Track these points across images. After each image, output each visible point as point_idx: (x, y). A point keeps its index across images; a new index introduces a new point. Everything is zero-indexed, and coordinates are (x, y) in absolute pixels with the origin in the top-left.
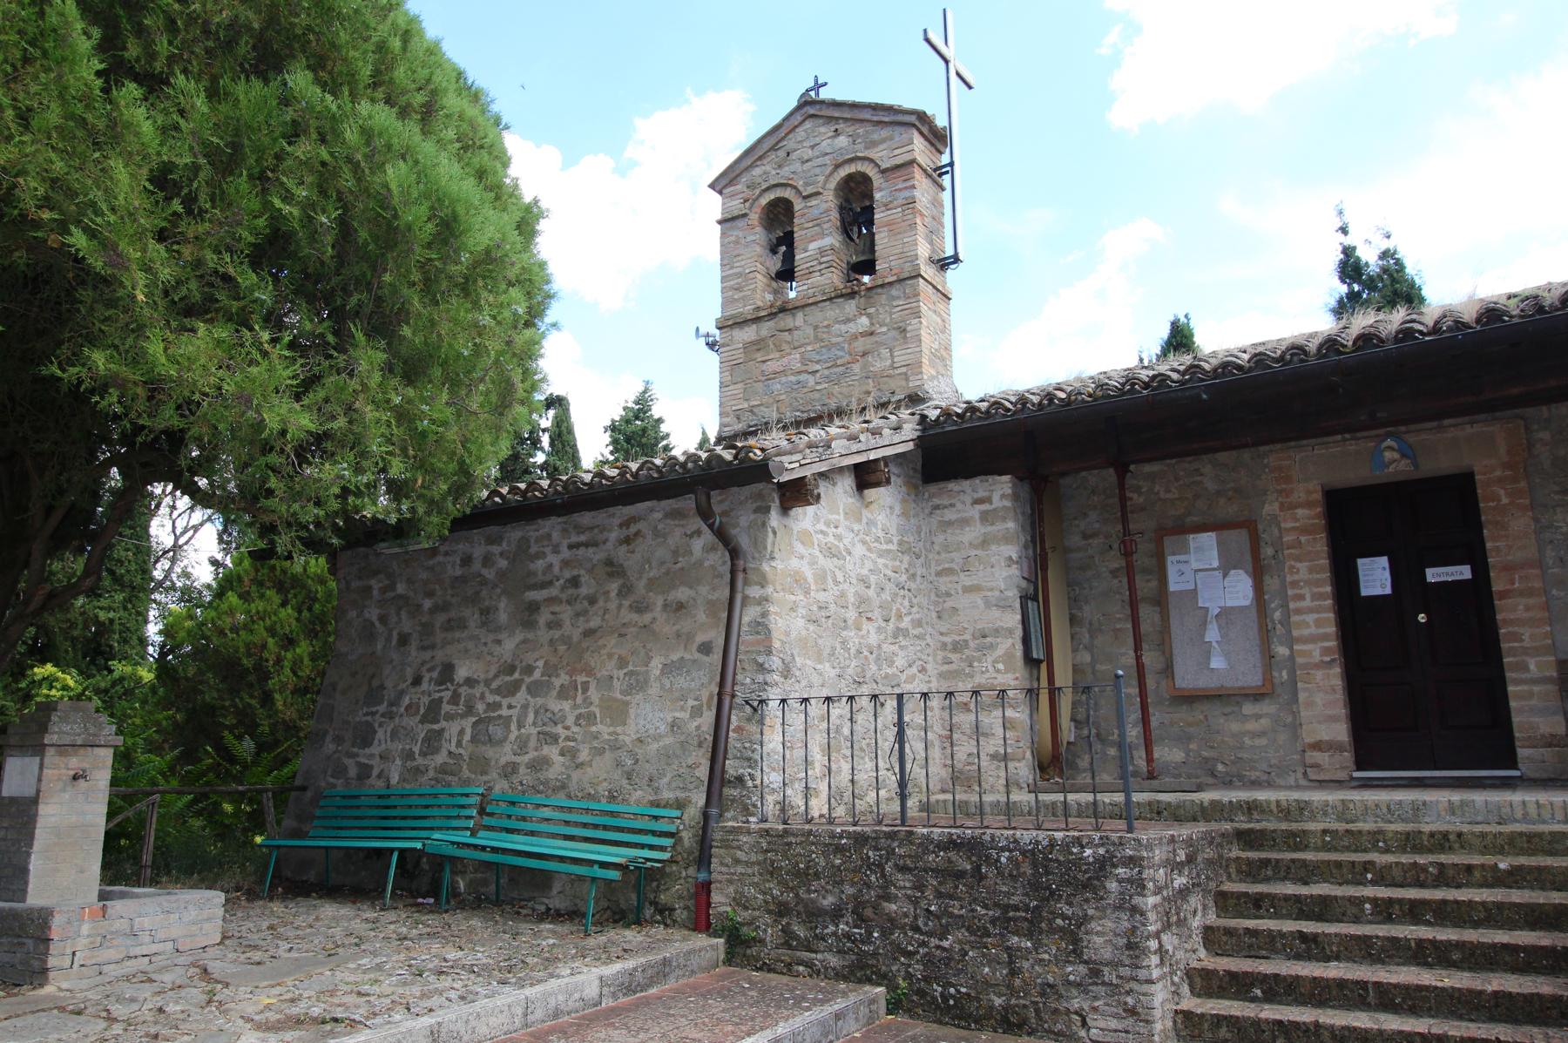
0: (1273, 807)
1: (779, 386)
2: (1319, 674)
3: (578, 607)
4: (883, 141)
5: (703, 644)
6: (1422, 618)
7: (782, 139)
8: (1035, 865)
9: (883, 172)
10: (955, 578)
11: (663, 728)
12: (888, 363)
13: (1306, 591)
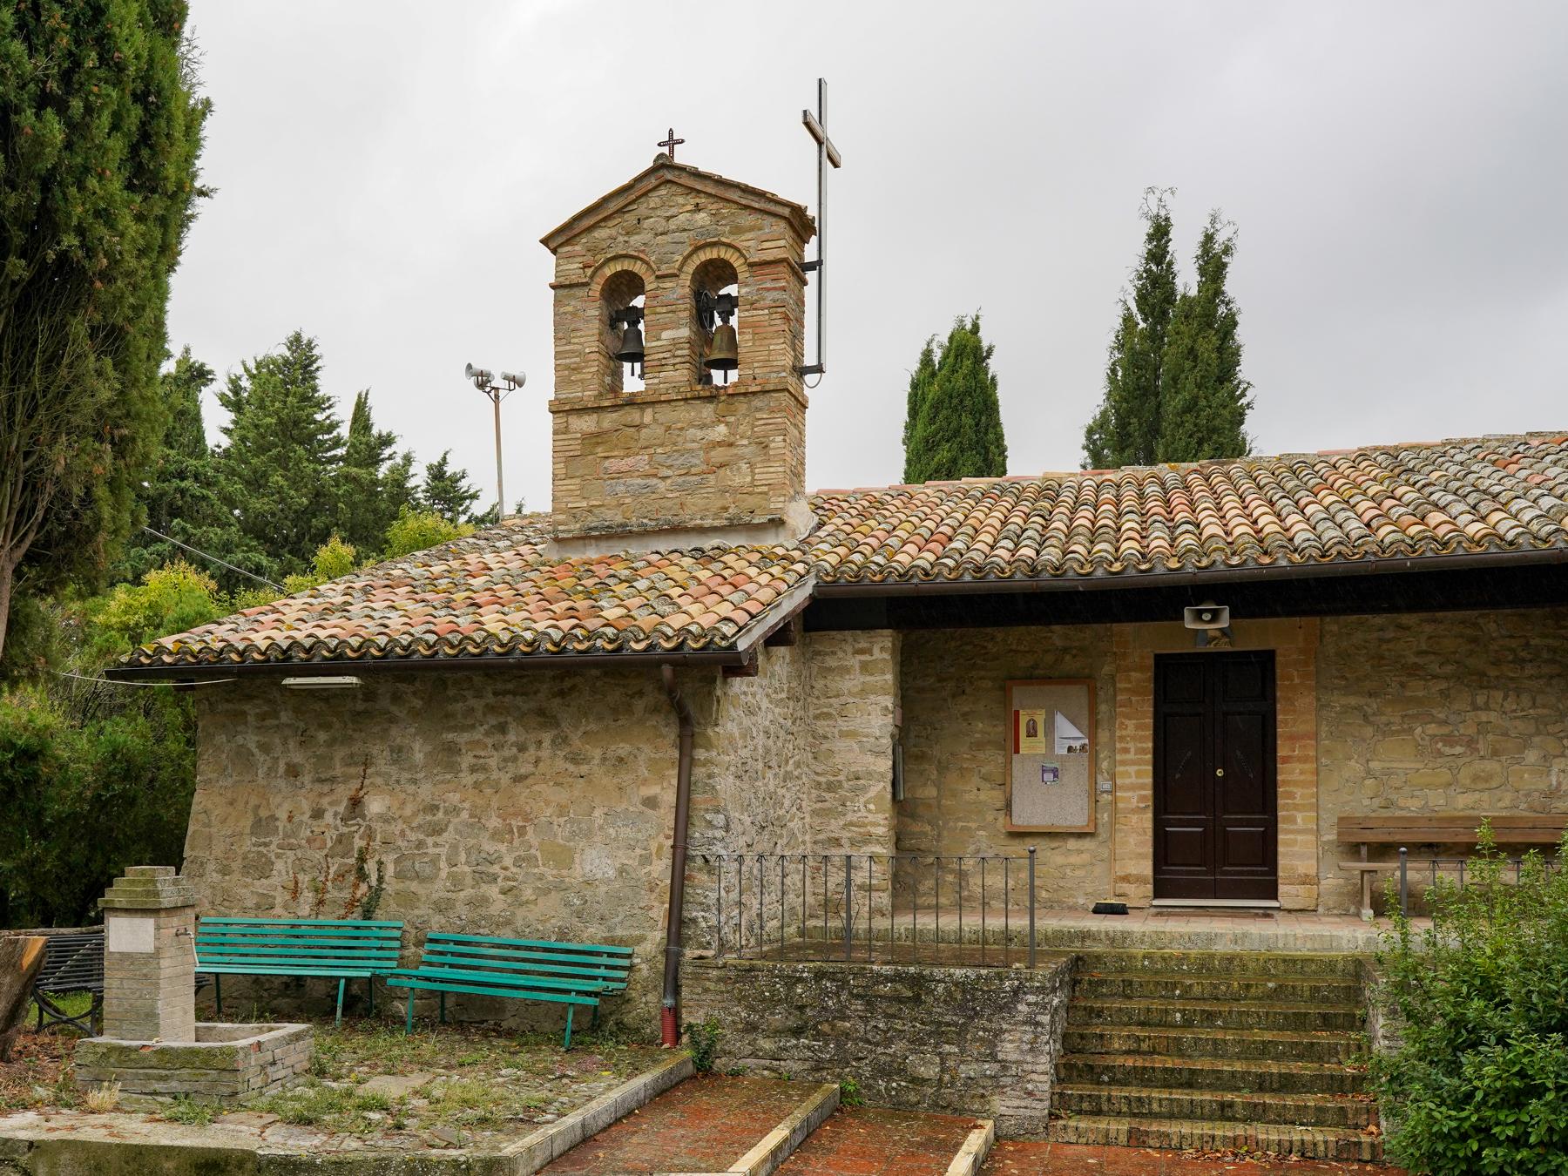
0: (1103, 936)
1: (623, 488)
2: (1134, 818)
3: (507, 753)
4: (751, 229)
5: (648, 798)
6: (1220, 773)
7: (633, 202)
8: (964, 992)
9: (751, 265)
10: (831, 723)
11: (611, 873)
12: (749, 479)
13: (1131, 746)
